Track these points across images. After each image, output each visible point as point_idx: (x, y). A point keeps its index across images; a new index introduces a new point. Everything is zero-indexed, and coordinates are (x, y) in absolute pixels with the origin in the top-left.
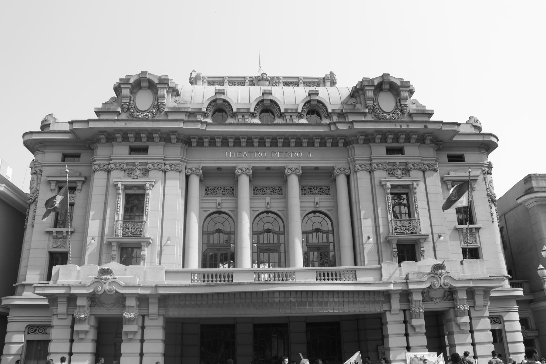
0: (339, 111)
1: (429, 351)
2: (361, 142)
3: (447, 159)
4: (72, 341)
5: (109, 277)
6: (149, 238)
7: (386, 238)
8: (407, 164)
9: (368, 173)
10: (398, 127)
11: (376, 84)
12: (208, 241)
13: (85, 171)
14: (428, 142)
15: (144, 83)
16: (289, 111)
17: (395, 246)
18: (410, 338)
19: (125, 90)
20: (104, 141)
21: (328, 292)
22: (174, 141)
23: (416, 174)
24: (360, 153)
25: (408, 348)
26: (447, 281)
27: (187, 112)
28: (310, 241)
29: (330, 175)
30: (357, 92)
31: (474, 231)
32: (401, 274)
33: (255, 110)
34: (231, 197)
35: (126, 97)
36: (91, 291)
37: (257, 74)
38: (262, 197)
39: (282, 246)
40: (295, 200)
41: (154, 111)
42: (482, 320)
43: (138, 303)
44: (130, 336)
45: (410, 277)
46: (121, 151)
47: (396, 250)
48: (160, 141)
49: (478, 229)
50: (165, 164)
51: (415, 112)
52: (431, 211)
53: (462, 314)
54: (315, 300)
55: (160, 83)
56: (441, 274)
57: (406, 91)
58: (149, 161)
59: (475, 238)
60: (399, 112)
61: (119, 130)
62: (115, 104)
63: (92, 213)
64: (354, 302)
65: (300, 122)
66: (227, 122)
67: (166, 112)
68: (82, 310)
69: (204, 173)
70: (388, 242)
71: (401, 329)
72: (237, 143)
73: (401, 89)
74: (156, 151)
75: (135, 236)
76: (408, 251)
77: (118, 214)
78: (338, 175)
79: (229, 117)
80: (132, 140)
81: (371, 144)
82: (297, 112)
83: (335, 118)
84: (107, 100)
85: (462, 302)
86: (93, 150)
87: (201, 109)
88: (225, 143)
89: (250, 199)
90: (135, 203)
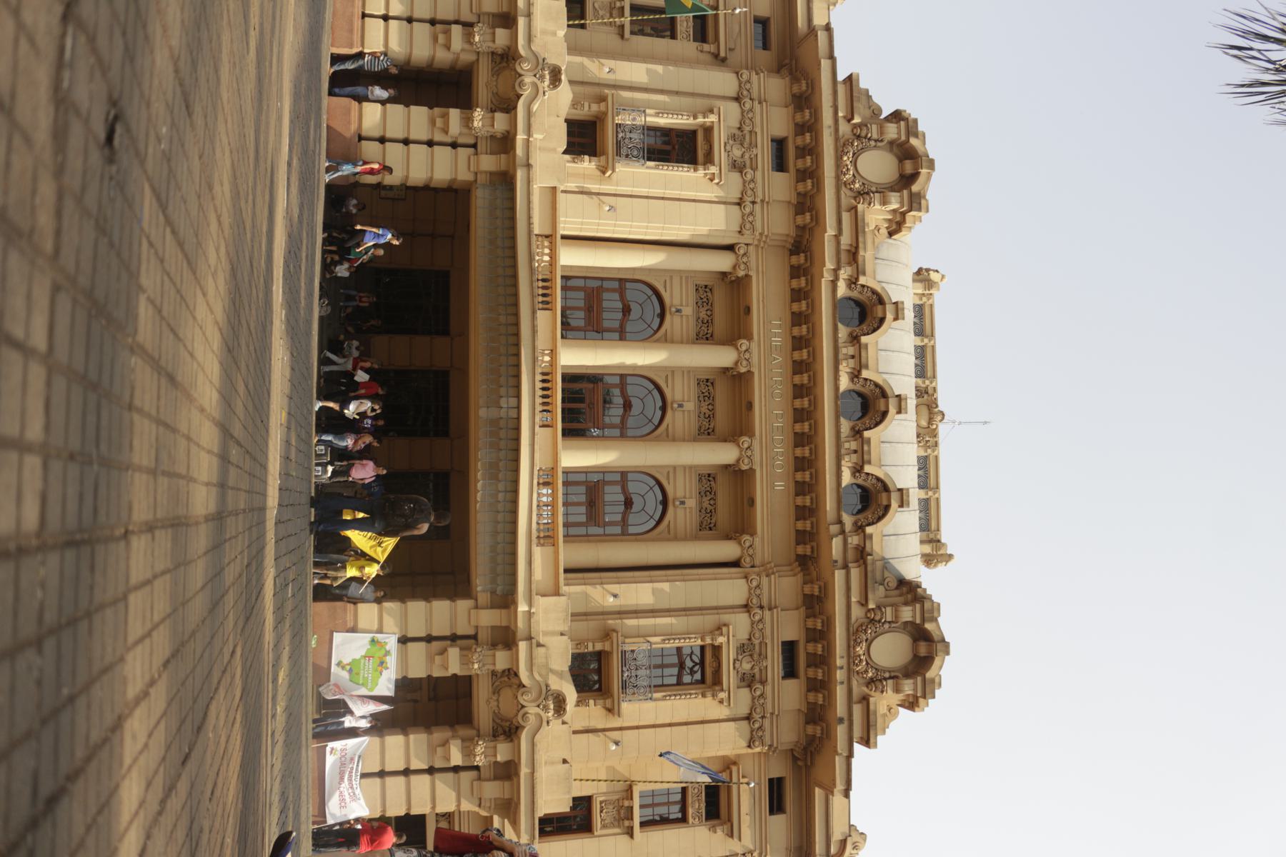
0: (868, 549)
1: (397, 681)
2: (807, 590)
3: (775, 775)
4: (433, 22)
5: (547, 82)
6: (613, 170)
7: (614, 630)
8: (763, 682)
9: (744, 602)
10: (839, 662)
11: (928, 626)
12: (608, 290)
13: (736, 58)
14: (810, 729)
15: (910, 166)
16: (866, 448)
17: (599, 647)
18: (423, 645)
19: (895, 130)
20: (796, 89)
21: (516, 482)
22: (800, 220)
23: (742, 700)
24: (786, 586)
25: (404, 640)
26: (532, 718)
27: (857, 248)
28: (607, 489)
29: (740, 527)
30: (910, 591)
31: (627, 823)
32: (546, 634)
33: (866, 379)
34: (692, 334)
35: (881, 132)
36: (522, 51)
37: (942, 405)
38: (695, 492)
39: (599, 531)
40: (684, 457)
41: (857, 185)
42: (454, 795)
43: (499, 135)
44: (439, 122)
45: (541, 650)
46: (777, 122)
47: (590, 649)
48: (799, 194)
49: (631, 835)
50: (753, 203)
51: (872, 707)
52: (668, 729)
53: (468, 752)
54: (502, 454)
55: (911, 195)
56: (546, 708)
57: (915, 689)
58: (759, 174)
59: (612, 825)
60: (870, 675)
61: (817, 115)
62: (868, 113)
63: (659, 68)
64: (495, 533)
65: (843, 468)
66: (840, 326)
67: (856, 208)
68: (489, 37)
69: (740, 375)
70: (607, 634)
71: (441, 629)
72: (799, 343)
73: (919, 679)
74: (779, 186)
75: (618, 145)
76: (584, 137)
77: (657, 115)
78: (740, 543)
79: (849, 330)
80: (799, 141)
81: (803, 609)
82: (863, 463)
83: (854, 540)
84: (876, 99)
85: (490, 752)
86: (778, 71)
87: (864, 274)
88: (798, 319)
89: (691, 467)
90: (677, 147)
